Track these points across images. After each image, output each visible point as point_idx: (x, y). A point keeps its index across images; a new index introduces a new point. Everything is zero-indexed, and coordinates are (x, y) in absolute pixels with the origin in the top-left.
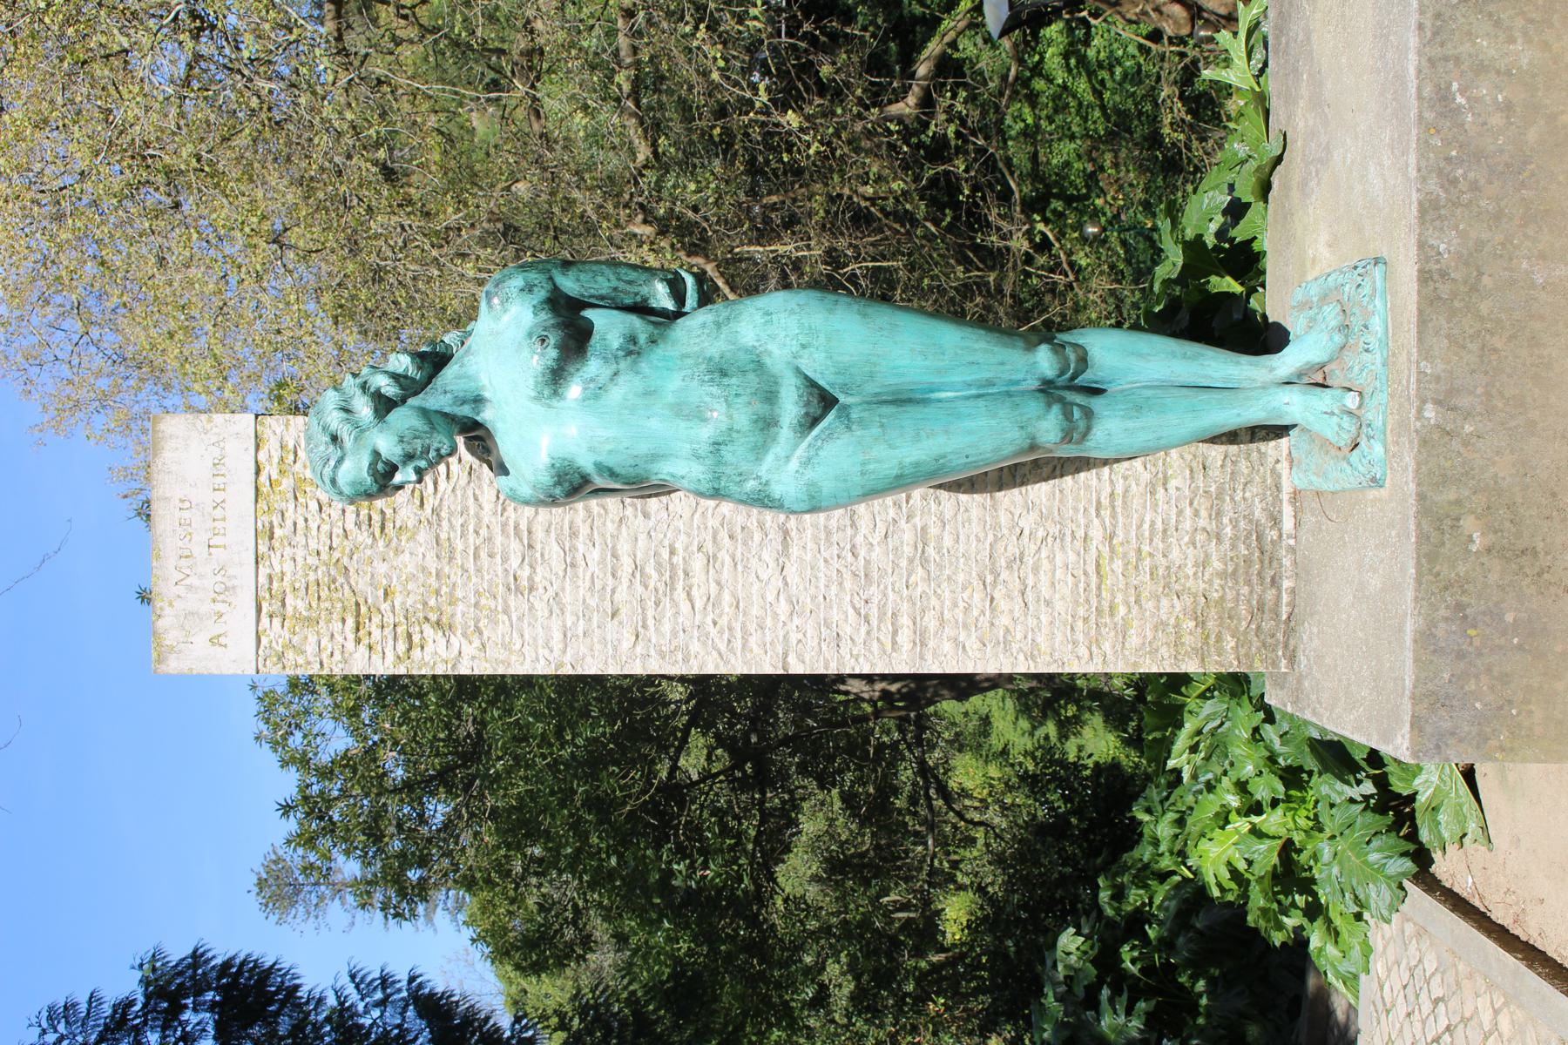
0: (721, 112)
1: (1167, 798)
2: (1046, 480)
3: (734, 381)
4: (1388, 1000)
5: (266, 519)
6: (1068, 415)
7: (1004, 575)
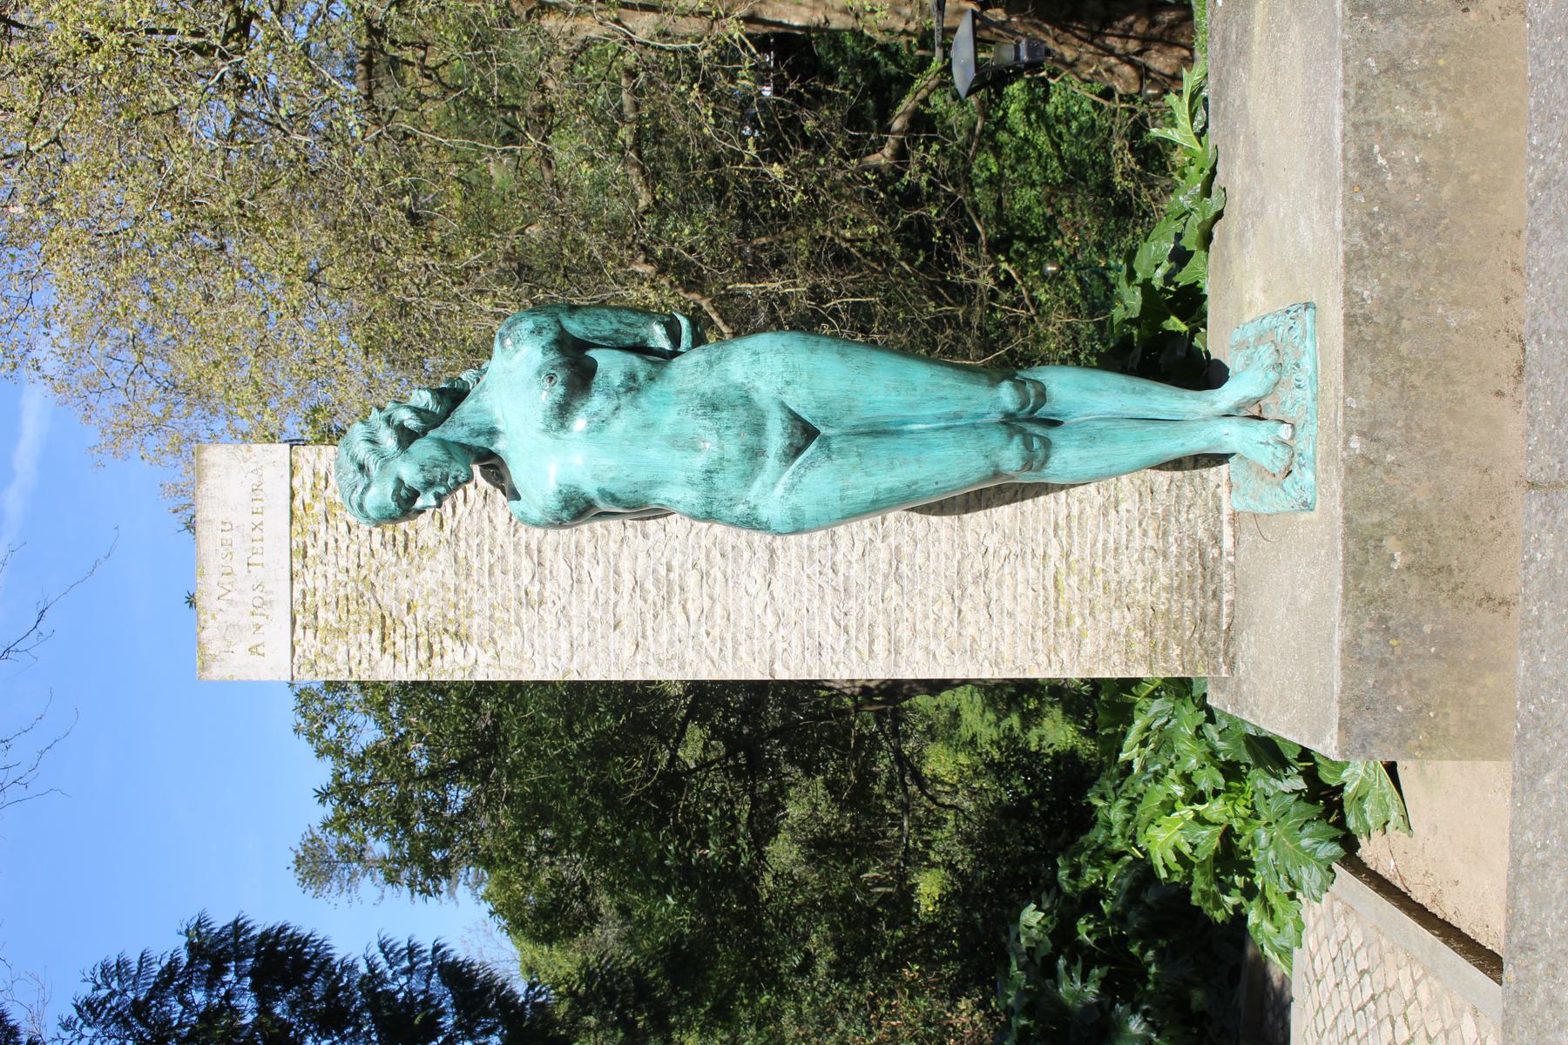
0: (716, 162)
1: (1120, 786)
2: (1008, 503)
3: (724, 414)
4: (1318, 972)
5: (299, 539)
6: (1028, 445)
7: (971, 589)
